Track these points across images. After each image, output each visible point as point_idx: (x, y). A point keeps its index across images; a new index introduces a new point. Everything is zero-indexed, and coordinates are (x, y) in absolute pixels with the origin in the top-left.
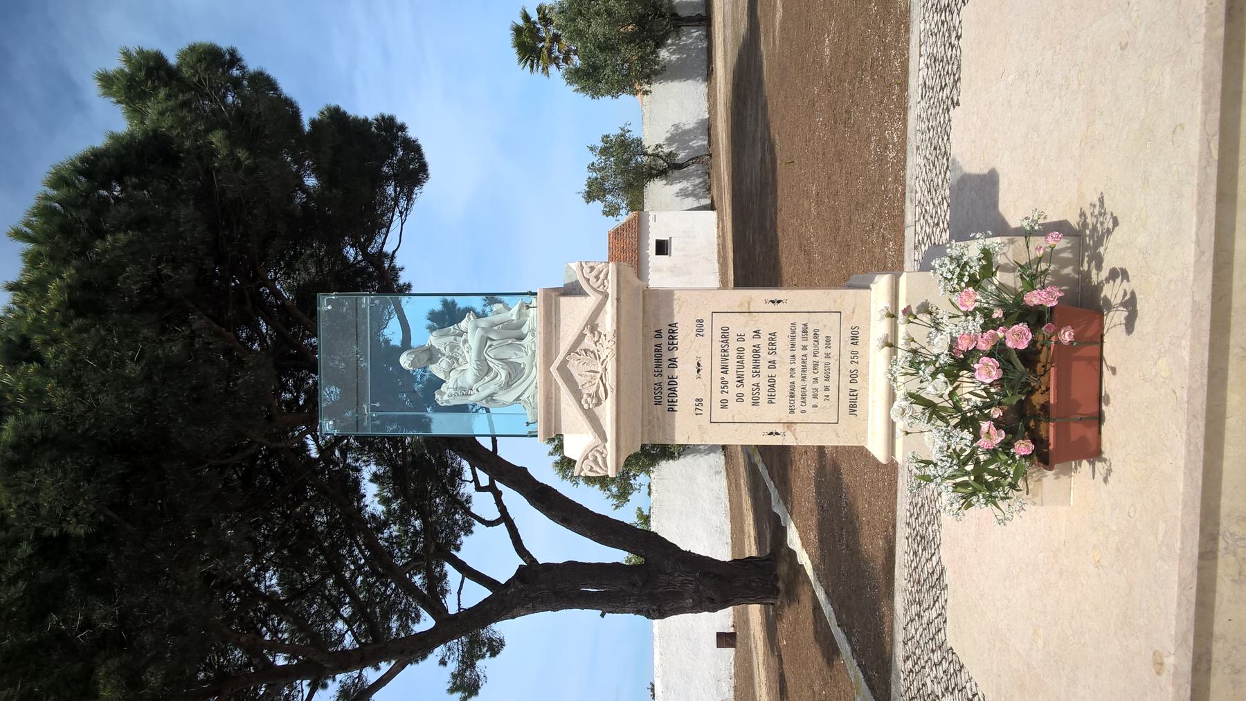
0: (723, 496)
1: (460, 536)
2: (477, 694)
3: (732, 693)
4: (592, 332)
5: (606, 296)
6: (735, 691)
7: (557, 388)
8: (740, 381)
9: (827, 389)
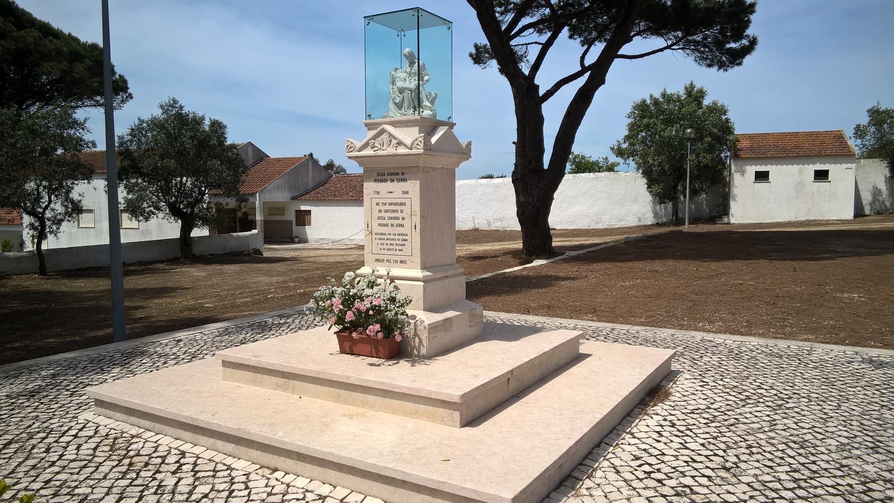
0: (622, 223)
1: (580, 37)
2: (475, 63)
3: (495, 229)
4: (397, 143)
5: (411, 149)
6: (496, 231)
7: (376, 129)
8: (386, 211)
9: (384, 249)
